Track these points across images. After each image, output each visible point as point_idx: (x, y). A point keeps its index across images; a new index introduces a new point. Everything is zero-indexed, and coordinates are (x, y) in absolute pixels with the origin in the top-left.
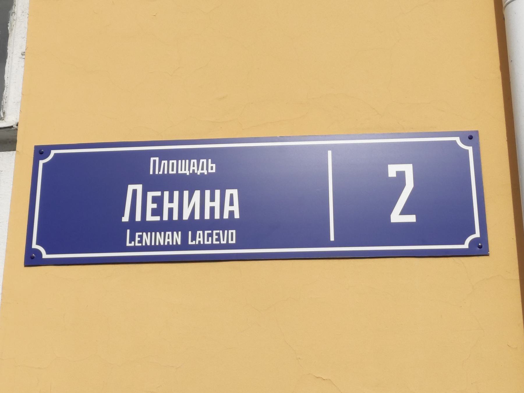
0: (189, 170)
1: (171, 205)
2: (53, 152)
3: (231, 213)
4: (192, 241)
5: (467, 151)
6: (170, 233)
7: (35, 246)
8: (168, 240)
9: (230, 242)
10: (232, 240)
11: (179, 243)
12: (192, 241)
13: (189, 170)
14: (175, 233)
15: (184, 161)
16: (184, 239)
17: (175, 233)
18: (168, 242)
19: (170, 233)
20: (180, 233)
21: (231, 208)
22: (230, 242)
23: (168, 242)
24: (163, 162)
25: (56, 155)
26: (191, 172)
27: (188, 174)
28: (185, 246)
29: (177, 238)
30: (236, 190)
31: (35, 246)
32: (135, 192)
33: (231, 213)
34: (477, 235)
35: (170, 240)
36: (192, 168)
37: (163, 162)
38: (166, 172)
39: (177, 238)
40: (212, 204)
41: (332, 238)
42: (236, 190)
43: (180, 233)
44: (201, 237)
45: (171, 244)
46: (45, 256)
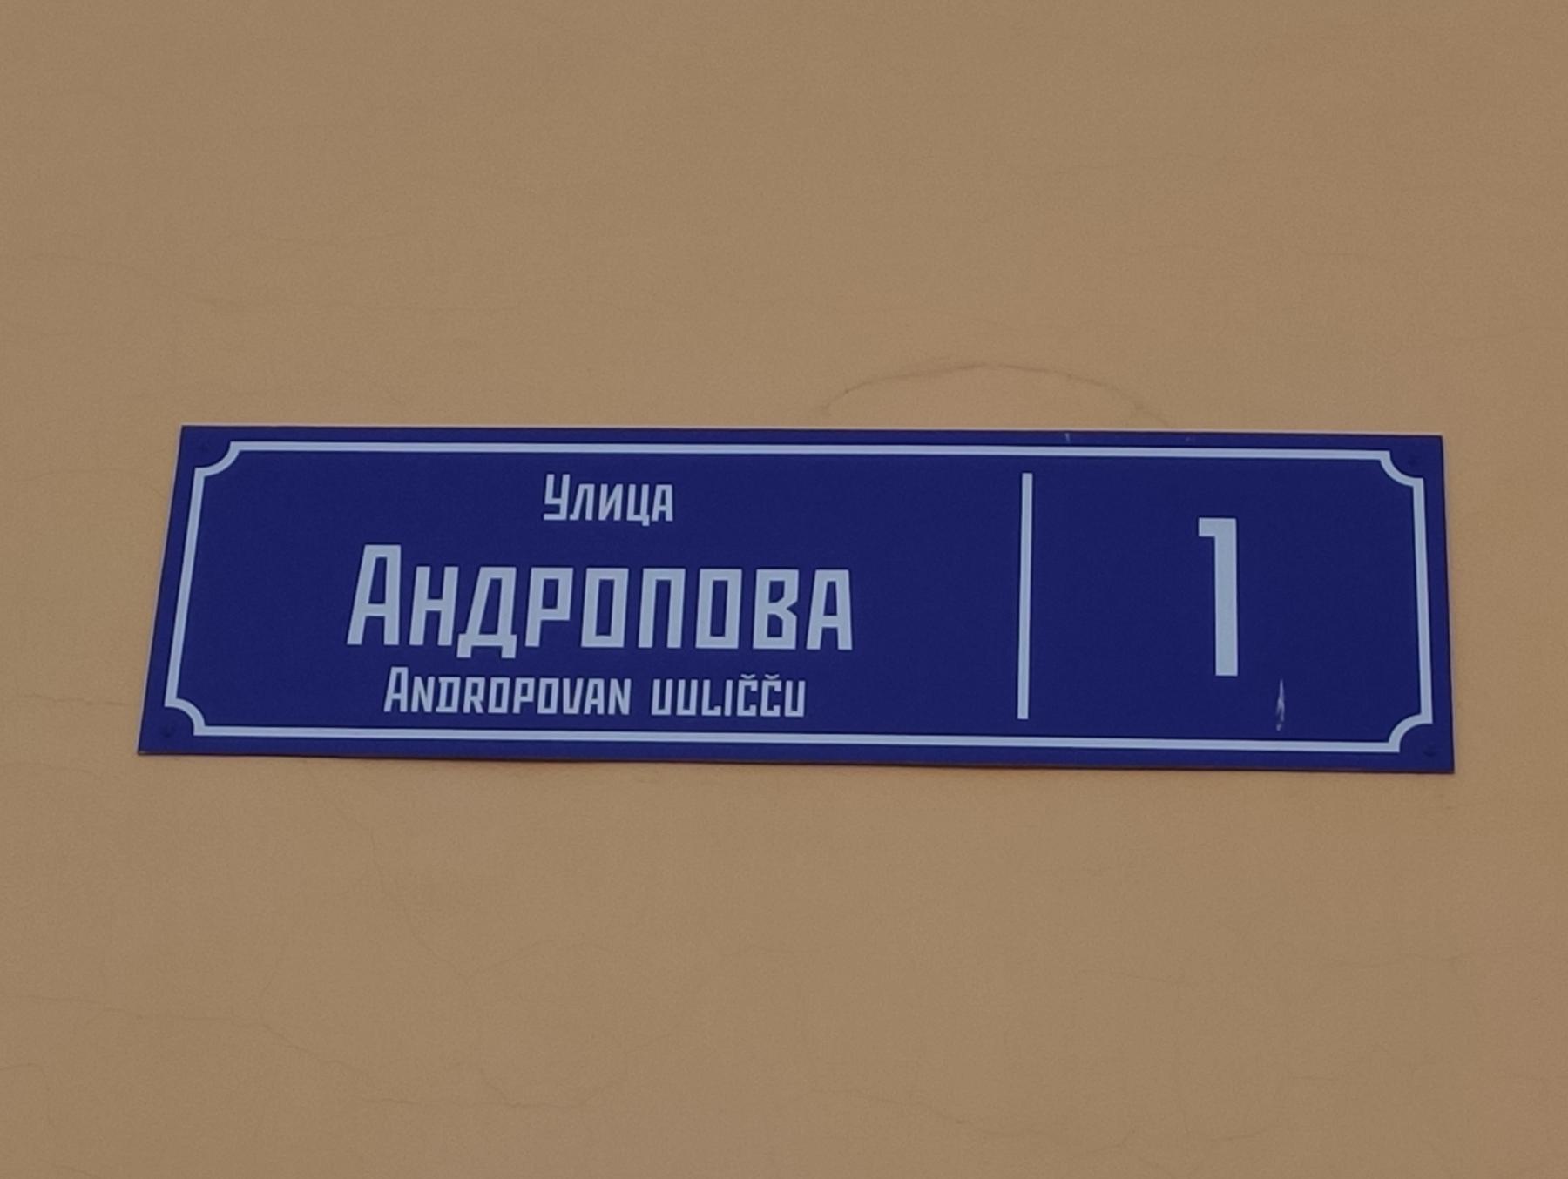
0: (650, 511)
1: (434, 606)
2: (236, 448)
3: (830, 635)
4: (711, 707)
5: (1410, 489)
6: (600, 683)
7: (172, 700)
8: (594, 702)
9: (681, 711)
10: (795, 707)
11: (625, 710)
12: (711, 707)
13: (650, 511)
14: (614, 683)
15: (632, 489)
16: (641, 698)
17: (614, 683)
18: (594, 708)
19: (600, 683)
20: (628, 683)
21: (830, 622)
22: (681, 711)
23: (594, 708)
24: (582, 487)
25: (243, 455)
26: (655, 517)
27: (646, 523)
28: (640, 717)
29: (621, 697)
30: (846, 573)
31: (172, 700)
32: (381, 564)
33: (830, 635)
34: (1425, 717)
35: (600, 702)
36: (657, 508)
37: (582, 487)
38: (589, 516)
39: (621, 697)
40: (434, 606)
41: (1023, 713)
42: (846, 573)
43: (628, 683)
44: (667, 698)
45: (601, 711)
46: (201, 729)
